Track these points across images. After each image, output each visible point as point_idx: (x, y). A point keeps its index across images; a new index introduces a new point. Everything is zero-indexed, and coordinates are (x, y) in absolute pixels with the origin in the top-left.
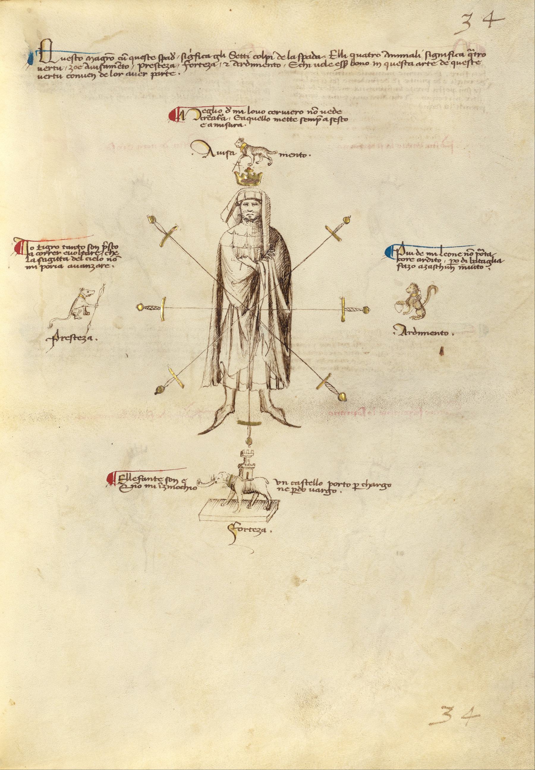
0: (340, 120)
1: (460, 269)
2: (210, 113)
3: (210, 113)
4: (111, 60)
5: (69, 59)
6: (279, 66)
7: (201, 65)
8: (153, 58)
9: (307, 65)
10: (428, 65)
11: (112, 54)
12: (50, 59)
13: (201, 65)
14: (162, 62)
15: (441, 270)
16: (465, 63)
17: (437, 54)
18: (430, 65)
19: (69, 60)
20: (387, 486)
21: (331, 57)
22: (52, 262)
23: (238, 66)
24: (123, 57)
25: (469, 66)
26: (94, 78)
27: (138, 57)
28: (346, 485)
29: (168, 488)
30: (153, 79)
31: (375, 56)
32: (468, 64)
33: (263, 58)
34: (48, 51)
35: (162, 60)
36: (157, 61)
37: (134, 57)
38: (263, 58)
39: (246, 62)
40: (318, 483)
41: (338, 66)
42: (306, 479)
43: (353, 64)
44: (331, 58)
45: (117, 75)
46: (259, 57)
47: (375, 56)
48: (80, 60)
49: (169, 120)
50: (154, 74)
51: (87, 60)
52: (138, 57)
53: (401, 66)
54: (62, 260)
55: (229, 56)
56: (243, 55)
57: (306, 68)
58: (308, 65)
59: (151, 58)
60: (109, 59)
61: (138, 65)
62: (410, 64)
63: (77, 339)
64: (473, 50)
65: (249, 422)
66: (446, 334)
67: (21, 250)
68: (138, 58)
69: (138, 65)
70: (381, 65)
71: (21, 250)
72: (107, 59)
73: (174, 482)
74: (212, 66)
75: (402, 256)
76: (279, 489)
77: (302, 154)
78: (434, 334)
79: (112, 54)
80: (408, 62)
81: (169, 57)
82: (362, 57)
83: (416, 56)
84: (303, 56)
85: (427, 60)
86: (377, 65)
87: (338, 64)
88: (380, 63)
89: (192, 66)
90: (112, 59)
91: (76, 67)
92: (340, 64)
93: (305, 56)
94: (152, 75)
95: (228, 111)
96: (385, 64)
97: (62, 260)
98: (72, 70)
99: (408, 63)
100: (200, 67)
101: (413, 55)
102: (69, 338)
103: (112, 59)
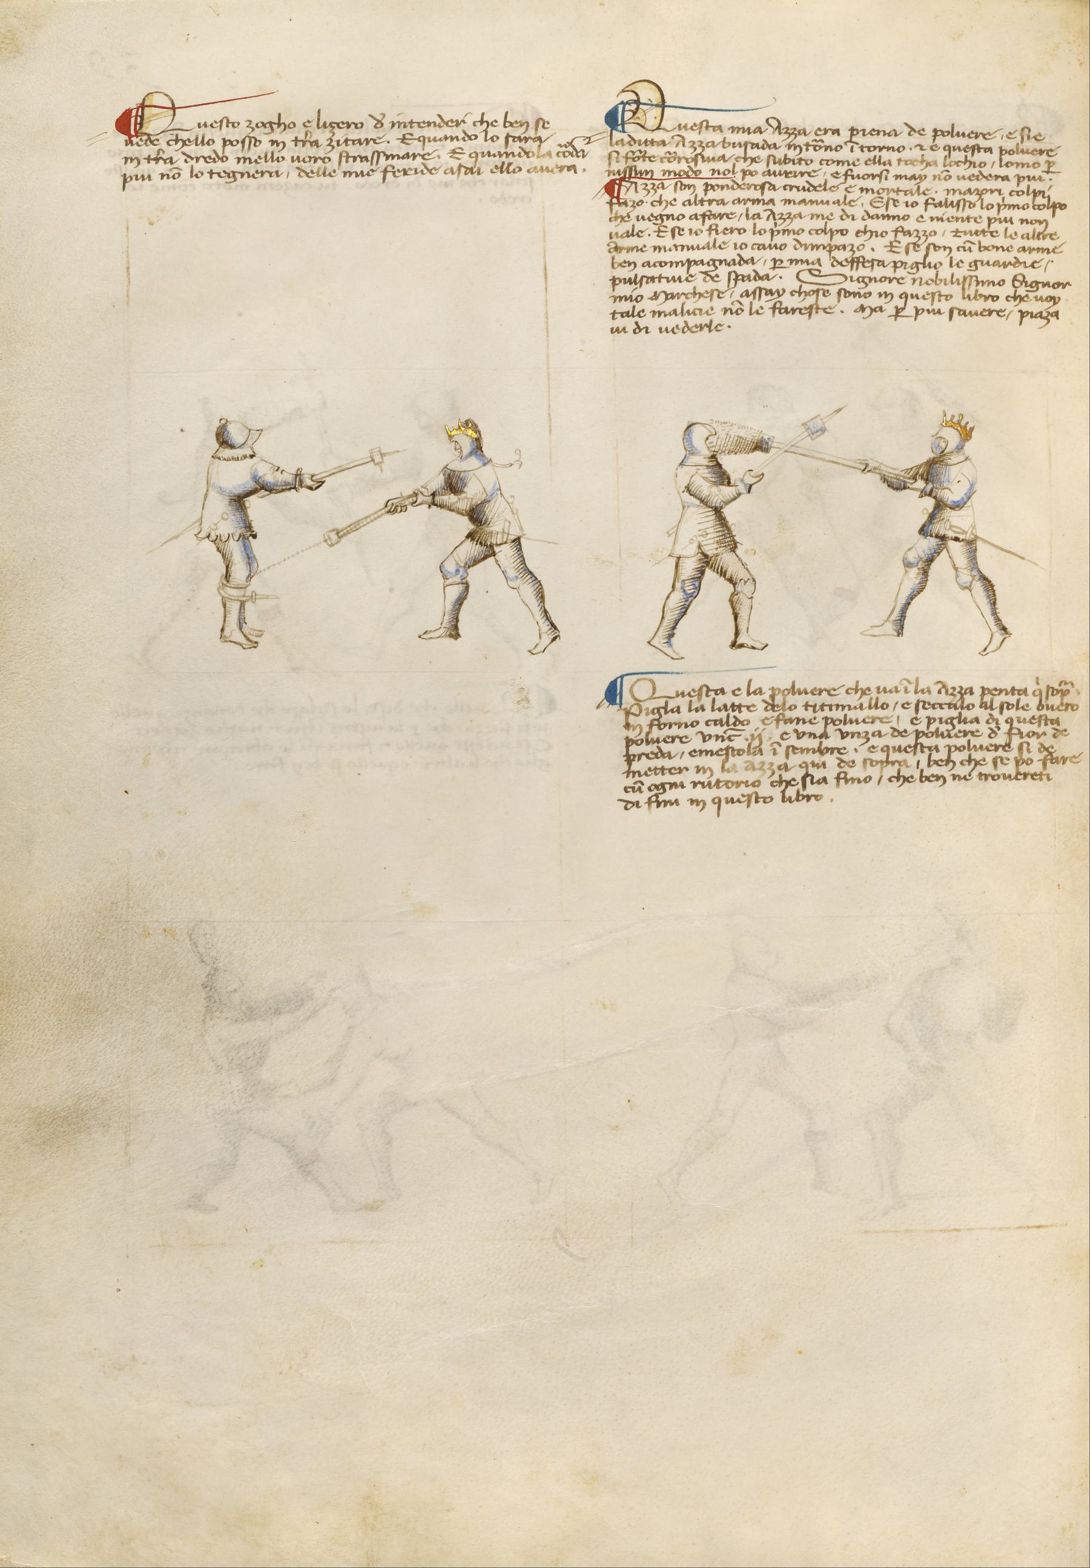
2: (865, 283)
3: (865, 283)
4: (993, 300)
5: (926, 297)
9: (872, 232)
12: (654, 693)
15: (702, 809)
17: (667, 783)
19: (925, 299)
20: (717, 263)
26: (703, 807)
32: (221, 126)
33: (826, 233)
37: (890, 746)
38: (826, 233)
39: (656, 750)
40: (880, 704)
46: (820, 232)
49: (604, 190)
51: (741, 296)
52: (732, 799)
55: (637, 95)
58: (874, 234)
60: (990, 778)
61: (691, 783)
67: (618, 697)
68: (1005, 777)
69: (691, 783)
71: (618, 697)
72: (668, 219)
73: (795, 149)
81: (749, 276)
84: (737, 276)
90: (995, 299)
92: (219, 124)
93: (941, 130)
96: (1034, 693)
101: (628, 312)
102: (724, 752)
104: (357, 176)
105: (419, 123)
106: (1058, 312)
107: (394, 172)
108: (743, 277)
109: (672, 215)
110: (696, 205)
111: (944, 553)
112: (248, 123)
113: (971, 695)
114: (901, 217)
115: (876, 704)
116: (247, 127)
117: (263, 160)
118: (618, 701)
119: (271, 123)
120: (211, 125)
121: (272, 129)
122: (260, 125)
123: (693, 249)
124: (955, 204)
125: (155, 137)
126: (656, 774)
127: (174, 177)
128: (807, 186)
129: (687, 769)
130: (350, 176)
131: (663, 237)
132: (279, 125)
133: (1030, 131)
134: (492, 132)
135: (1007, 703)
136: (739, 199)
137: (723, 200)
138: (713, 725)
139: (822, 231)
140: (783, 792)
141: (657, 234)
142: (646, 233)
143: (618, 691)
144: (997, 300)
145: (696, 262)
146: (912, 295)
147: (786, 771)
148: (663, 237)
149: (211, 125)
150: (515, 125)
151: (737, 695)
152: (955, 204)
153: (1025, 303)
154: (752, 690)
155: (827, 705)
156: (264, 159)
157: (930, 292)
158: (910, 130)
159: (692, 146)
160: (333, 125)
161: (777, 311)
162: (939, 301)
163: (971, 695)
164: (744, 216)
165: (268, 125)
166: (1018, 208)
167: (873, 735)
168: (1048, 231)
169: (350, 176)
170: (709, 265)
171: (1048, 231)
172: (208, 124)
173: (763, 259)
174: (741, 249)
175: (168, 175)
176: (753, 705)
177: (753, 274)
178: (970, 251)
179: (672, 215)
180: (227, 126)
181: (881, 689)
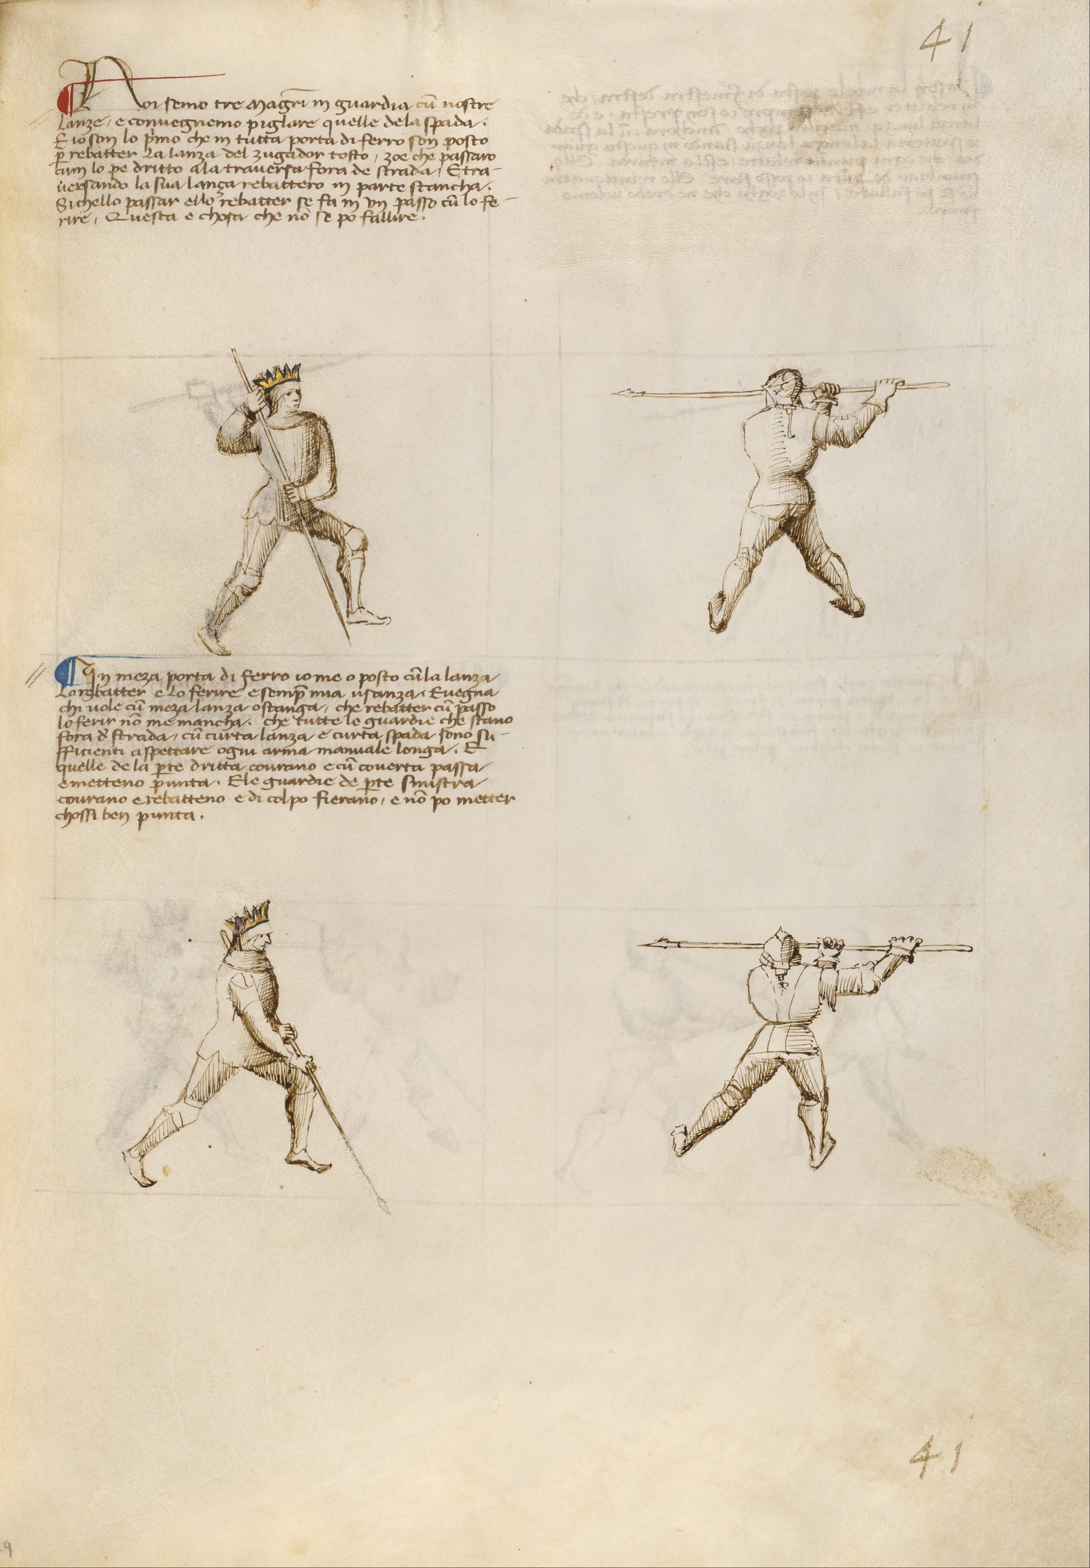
1: (151, 710)
6: (394, 678)
7: (322, 141)
8: (412, 217)
10: (320, 143)
11: (311, 1117)
16: (211, 123)
21: (433, 694)
24: (347, 764)
25: (425, 209)
27: (383, 766)
29: (241, 754)
30: (142, 828)
31: (278, 679)
44: (432, 696)
45: (312, 155)
46: (260, 768)
47: (316, 142)
50: (366, 678)
52: (383, 766)
54: (196, 784)
57: (262, 112)
66: (178, 170)
70: (229, 142)
75: (151, 745)
77: (172, 166)
79: (311, 1117)
81: (406, 170)
82: (365, 753)
83: (378, 751)
84: (153, 750)
85: (301, 209)
86: (379, 205)
88: (227, 138)
94: (142, 818)
97: (196, 784)
98: (260, 158)
100: (391, 190)
103: (319, 186)
104: (195, 107)
106: (487, 168)
107: (319, 169)
111: (939, 41)
112: (256, 153)
114: (134, 783)
115: (365, 123)
117: (260, 185)
118: (69, 110)
121: (345, 110)
124: (475, 708)
125: (675, 175)
126: (99, 786)
127: (134, 724)
129: (323, 155)
130: (162, 142)
131: (236, 786)
134: (353, 716)
138: (225, 187)
139: (463, 140)
140: (348, 716)
141: (56, 144)
142: (106, 121)
143: (70, 674)
144: (322, 187)
145: (368, 187)
148: (236, 786)
152: (475, 708)
153: (207, 143)
156: (357, 123)
157: (96, 780)
164: (260, 736)
165: (184, 123)
166: (115, 802)
167: (299, 738)
168: (303, 718)
169: (162, 142)
171: (303, 718)
173: (325, 707)
174: (174, 142)
175: (128, 721)
176: (285, 720)
180: (386, 174)
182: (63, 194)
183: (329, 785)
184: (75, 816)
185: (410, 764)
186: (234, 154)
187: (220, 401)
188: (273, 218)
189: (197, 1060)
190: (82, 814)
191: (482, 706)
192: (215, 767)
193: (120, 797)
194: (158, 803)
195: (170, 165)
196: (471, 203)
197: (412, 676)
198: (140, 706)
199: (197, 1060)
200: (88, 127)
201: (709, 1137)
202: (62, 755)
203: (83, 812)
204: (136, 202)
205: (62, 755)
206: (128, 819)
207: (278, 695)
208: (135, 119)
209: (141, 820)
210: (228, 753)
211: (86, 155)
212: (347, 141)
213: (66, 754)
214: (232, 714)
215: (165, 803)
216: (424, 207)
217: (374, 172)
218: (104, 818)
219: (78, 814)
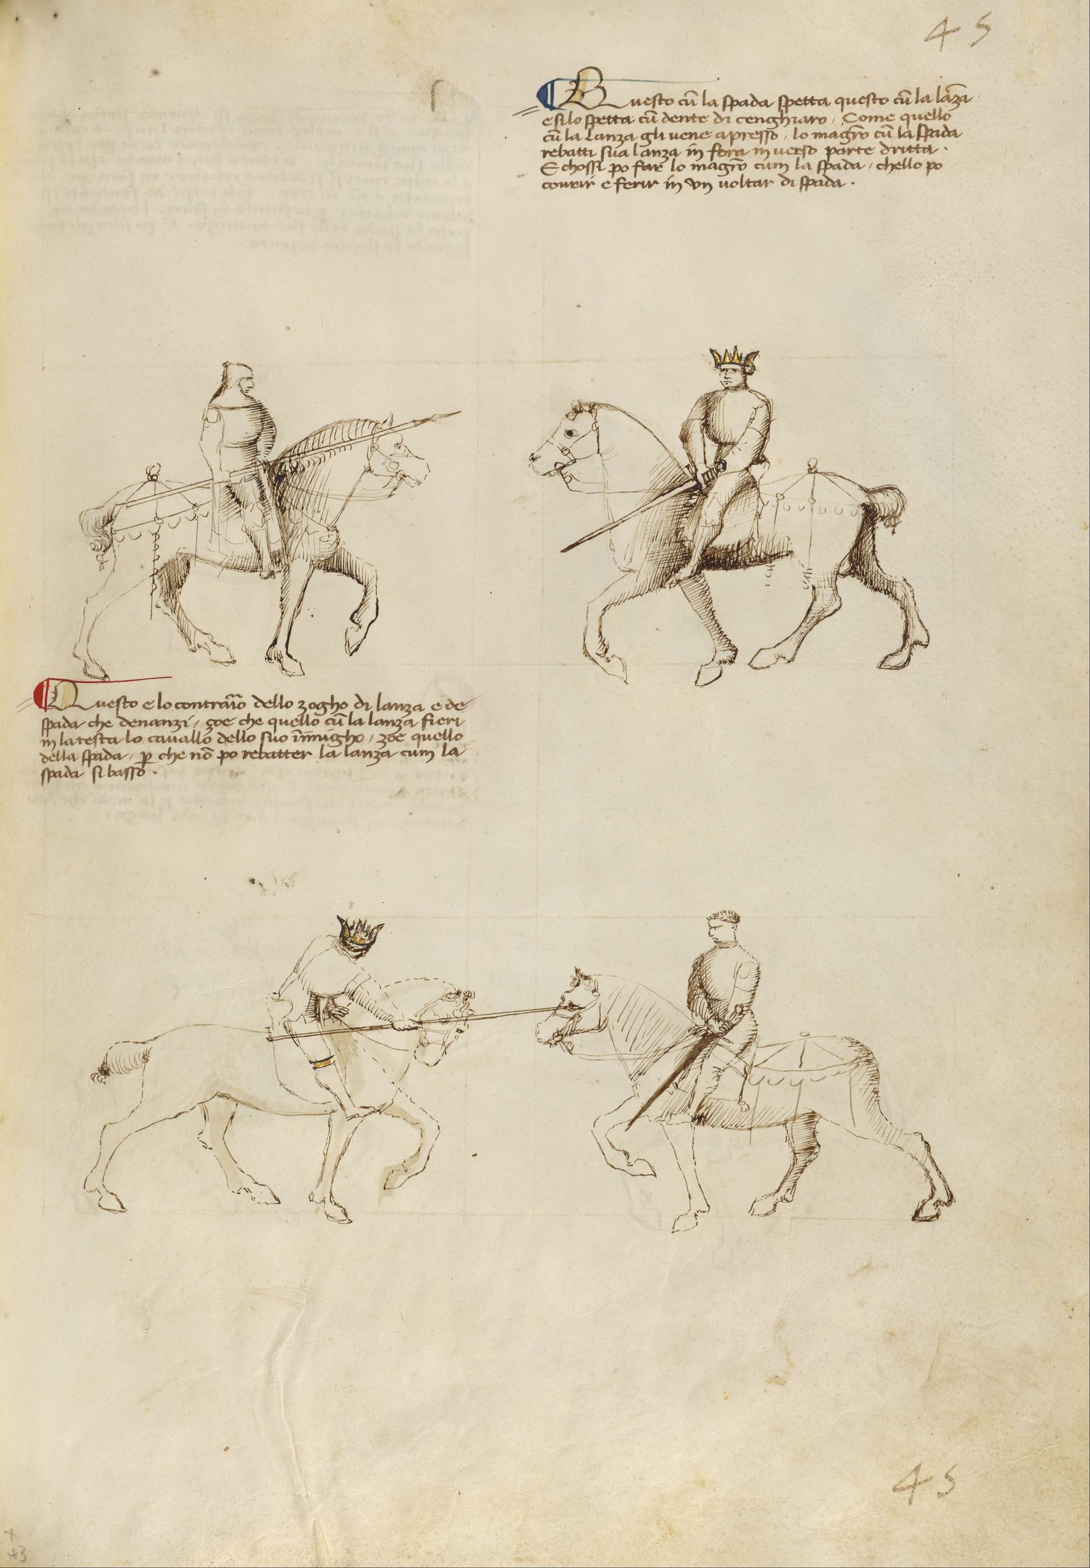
0: (657, 102)
10: (859, 153)
13: (82, 741)
14: (925, 141)
18: (862, 152)
22: (410, 713)
23: (268, 758)
28: (697, 119)
32: (95, 742)
34: (358, 703)
35: (732, 106)
36: (774, 111)
41: (648, 104)
42: (873, 94)
43: (112, 773)
48: (667, 104)
53: (759, 139)
56: (809, 98)
59: (666, 101)
62: (757, 184)
63: (663, 102)
64: (239, 696)
65: (734, 139)
74: (626, 140)
76: (239, 696)
78: (688, 136)
80: (74, 771)
84: (927, 130)
87: (648, 102)
89: (187, 706)
91: (313, 706)
95: (141, 773)
99: (106, 738)
100: (918, 152)
105: (86, 740)
108: (933, 132)
109: (696, 134)
110: (308, 725)
113: (829, 147)
116: (299, 707)
119: (324, 704)
120: (435, 737)
122: (313, 706)
123: (677, 138)
128: (750, 100)
132: (332, 705)
133: (101, 770)
135: (810, 147)
136: (389, 704)
137: (825, 100)
146: (281, 720)
147: (930, 154)
149: (109, 705)
150: (602, 121)
151: (869, 154)
154: (352, 721)
155: (862, 149)
158: (42, 757)
159: (177, 724)
160: (340, 738)
161: (621, 186)
162: (874, 103)
163: (829, 147)
167: (414, 709)
170: (842, 137)
172: (107, 703)
177: (942, 129)
178: (694, 104)
179: (696, 134)
181: (779, 150)
182: (49, 764)
183: (606, 188)
184: (581, 168)
185: (862, 148)
186: (227, 739)
187: (849, 136)
188: (177, 756)
189: (81, 725)
190: (588, 167)
191: (130, 770)
192: (905, 150)
193: (171, 708)
194: (602, 124)
195: (694, 114)
196: (678, 169)
197: (334, 720)
198: (340, 720)
199: (81, 725)
200: (407, 711)
201: (450, 417)
202: (45, 731)
203: (588, 164)
204: (196, 704)
205: (45, 731)
206: (431, 759)
207: (140, 725)
208: (743, 118)
209: (929, 168)
210: (318, 708)
211: (558, 153)
212: (71, 774)
213: (48, 732)
214: (305, 710)
215: (609, 123)
216: (593, 168)
217: (815, 167)
218: (109, 776)
219: (583, 166)
